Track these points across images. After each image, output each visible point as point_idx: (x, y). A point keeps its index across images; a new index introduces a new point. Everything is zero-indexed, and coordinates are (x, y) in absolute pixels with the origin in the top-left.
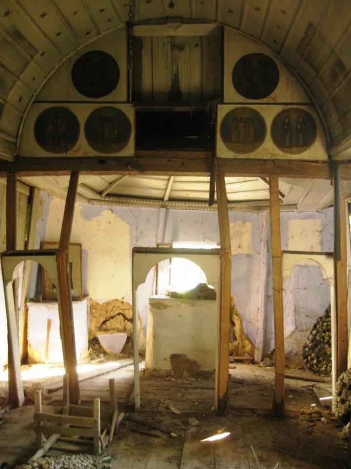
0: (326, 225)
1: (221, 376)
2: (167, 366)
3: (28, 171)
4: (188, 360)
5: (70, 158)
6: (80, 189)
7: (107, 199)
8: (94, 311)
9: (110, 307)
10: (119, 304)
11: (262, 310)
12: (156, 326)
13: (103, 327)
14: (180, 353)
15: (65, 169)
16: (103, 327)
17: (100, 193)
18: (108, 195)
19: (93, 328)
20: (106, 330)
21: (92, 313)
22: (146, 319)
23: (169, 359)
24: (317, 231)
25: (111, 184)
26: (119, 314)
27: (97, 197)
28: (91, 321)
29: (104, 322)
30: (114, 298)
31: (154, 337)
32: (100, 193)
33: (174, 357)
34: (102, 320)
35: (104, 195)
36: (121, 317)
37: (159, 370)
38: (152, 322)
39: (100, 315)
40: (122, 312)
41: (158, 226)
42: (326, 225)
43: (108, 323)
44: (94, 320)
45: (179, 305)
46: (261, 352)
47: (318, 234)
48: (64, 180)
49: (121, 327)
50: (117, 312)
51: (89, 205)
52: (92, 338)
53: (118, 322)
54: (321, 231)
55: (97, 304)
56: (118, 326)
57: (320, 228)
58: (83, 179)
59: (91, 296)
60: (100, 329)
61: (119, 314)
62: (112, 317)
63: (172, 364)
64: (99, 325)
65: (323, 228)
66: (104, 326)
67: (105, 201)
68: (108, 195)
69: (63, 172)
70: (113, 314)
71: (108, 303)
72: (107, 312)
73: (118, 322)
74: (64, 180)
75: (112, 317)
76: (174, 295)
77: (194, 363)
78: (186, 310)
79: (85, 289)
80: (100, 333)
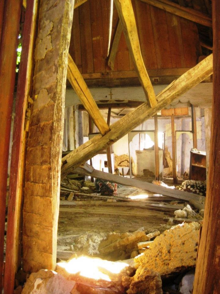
0: (203, 123)
1: (157, 170)
2: (142, 174)
3: (199, 62)
4: (149, 171)
5: (108, 104)
6: (112, 114)
7: (120, 116)
8: (116, 159)
9: (122, 158)
10: (126, 156)
11: (181, 157)
12: (138, 160)
13: (119, 165)
14: (147, 169)
15: (107, 107)
16: (119, 165)
17: (117, 114)
18: (121, 115)
19: (116, 165)
20: (121, 166)
21: (115, 160)
22: (134, 157)
23: (143, 171)
24: (200, 126)
25: (121, 111)
26: (126, 160)
27: (116, 116)
28: (115, 162)
29: (120, 163)
30: (124, 154)
31: (137, 163)
32: (117, 114)
33: (145, 170)
34: (119, 162)
35: (119, 115)
36: (126, 161)
37: (139, 175)
38: (137, 158)
39: (119, 160)
40: (127, 159)
41: (155, 147)
42: (203, 123)
43: (122, 164)
44: (116, 162)
45: (146, 152)
46: (180, 174)
47: (200, 127)
48: (106, 111)
49: (127, 165)
50: (125, 159)
51: (113, 119)
52: (115, 169)
53: (125, 163)
54: (201, 126)
55: (117, 156)
56: (125, 164)
57: (201, 125)
58: (113, 110)
59: (115, 153)
60: (119, 165)
61: (126, 160)
62: (123, 161)
63: (144, 173)
64: (118, 164)
65: (202, 124)
66: (120, 164)
67: (119, 117)
68: (121, 115)
69: (106, 108)
70: (123, 160)
71: (121, 156)
72: (121, 159)
73: (125, 163)
74: (106, 111)
75: (123, 161)
76: (144, 149)
77: (151, 172)
78: (148, 153)
79: (113, 150)
80: (119, 167)
